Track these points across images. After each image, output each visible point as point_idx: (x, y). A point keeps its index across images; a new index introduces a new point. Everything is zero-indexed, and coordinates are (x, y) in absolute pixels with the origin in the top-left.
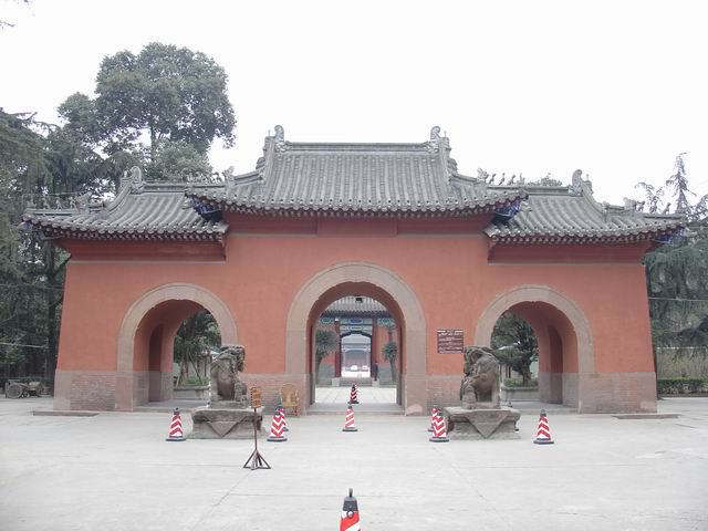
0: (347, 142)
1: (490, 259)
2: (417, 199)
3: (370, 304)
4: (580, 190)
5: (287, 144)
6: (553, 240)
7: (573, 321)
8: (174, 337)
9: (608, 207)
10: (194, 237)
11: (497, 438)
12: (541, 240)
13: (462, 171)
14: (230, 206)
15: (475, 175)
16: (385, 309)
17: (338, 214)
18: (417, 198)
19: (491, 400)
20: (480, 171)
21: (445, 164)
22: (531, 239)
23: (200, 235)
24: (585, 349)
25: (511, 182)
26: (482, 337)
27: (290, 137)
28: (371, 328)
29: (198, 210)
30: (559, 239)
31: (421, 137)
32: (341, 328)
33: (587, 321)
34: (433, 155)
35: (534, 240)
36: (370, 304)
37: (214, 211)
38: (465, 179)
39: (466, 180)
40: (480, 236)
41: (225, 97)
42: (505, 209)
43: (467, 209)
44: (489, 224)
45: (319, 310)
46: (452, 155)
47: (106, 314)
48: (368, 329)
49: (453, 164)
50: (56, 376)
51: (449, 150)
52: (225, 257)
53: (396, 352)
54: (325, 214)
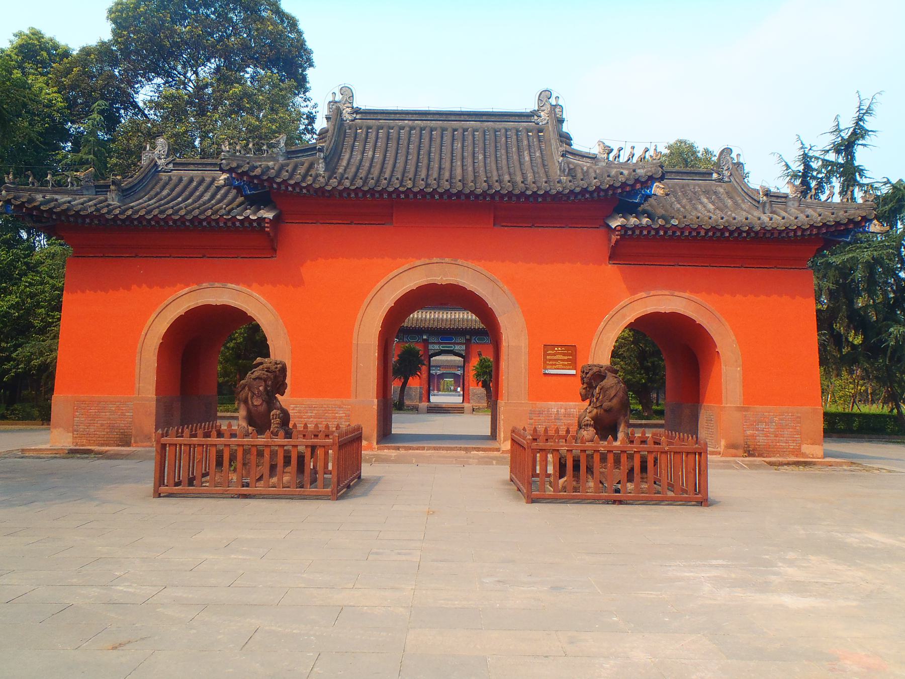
0: (457, 109)
1: (610, 258)
2: (519, 179)
3: (466, 317)
4: (721, 172)
5: (357, 111)
6: (694, 234)
7: (716, 338)
8: (214, 366)
9: (767, 193)
10: (234, 224)
11: (355, 496)
12: (678, 233)
13: (578, 145)
14: (279, 184)
15: (595, 150)
16: (482, 326)
17: (419, 197)
18: (519, 179)
19: (44, 417)
20: (601, 143)
21: (554, 142)
22: (682, 233)
23: (191, 221)
24: (729, 375)
25: (642, 159)
26: (601, 354)
27: (362, 102)
28: (464, 347)
29: (239, 190)
30: (702, 233)
31: (528, 105)
32: (430, 347)
33: (734, 338)
34: (539, 128)
35: (670, 233)
36: (466, 317)
37: (257, 189)
38: (582, 156)
39: (583, 156)
40: (602, 229)
41: (86, 52)
42: (633, 192)
43: (584, 191)
44: (625, 214)
45: (394, 324)
46: (565, 128)
47: (116, 335)
48: (460, 348)
49: (566, 139)
50: (710, 479)
51: (561, 121)
52: (275, 251)
53: (490, 378)
54: (402, 196)
